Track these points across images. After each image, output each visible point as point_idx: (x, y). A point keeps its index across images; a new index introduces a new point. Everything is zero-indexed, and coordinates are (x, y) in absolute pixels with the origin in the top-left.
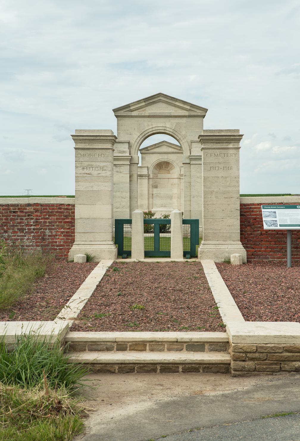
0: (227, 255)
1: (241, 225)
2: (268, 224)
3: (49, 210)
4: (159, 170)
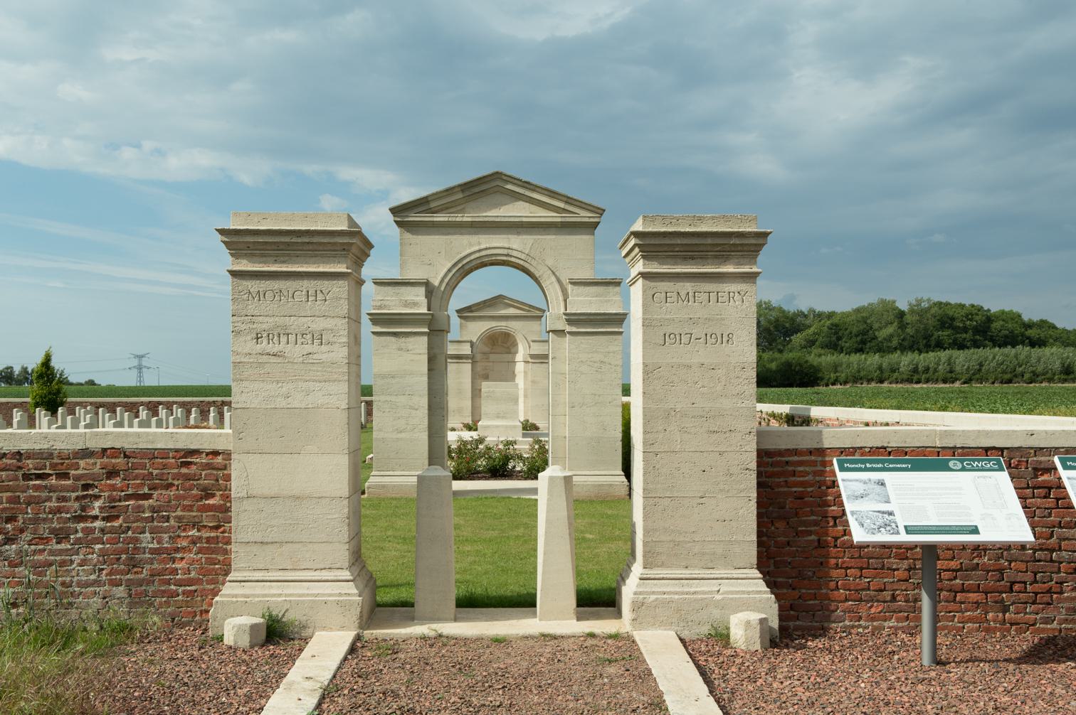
0: (716, 613)
1: (759, 516)
2: (865, 525)
3: (151, 470)
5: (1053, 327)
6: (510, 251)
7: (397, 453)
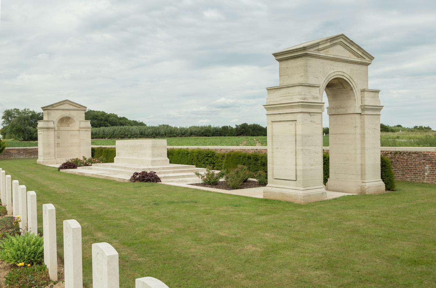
4: (60, 123)
5: (127, 119)
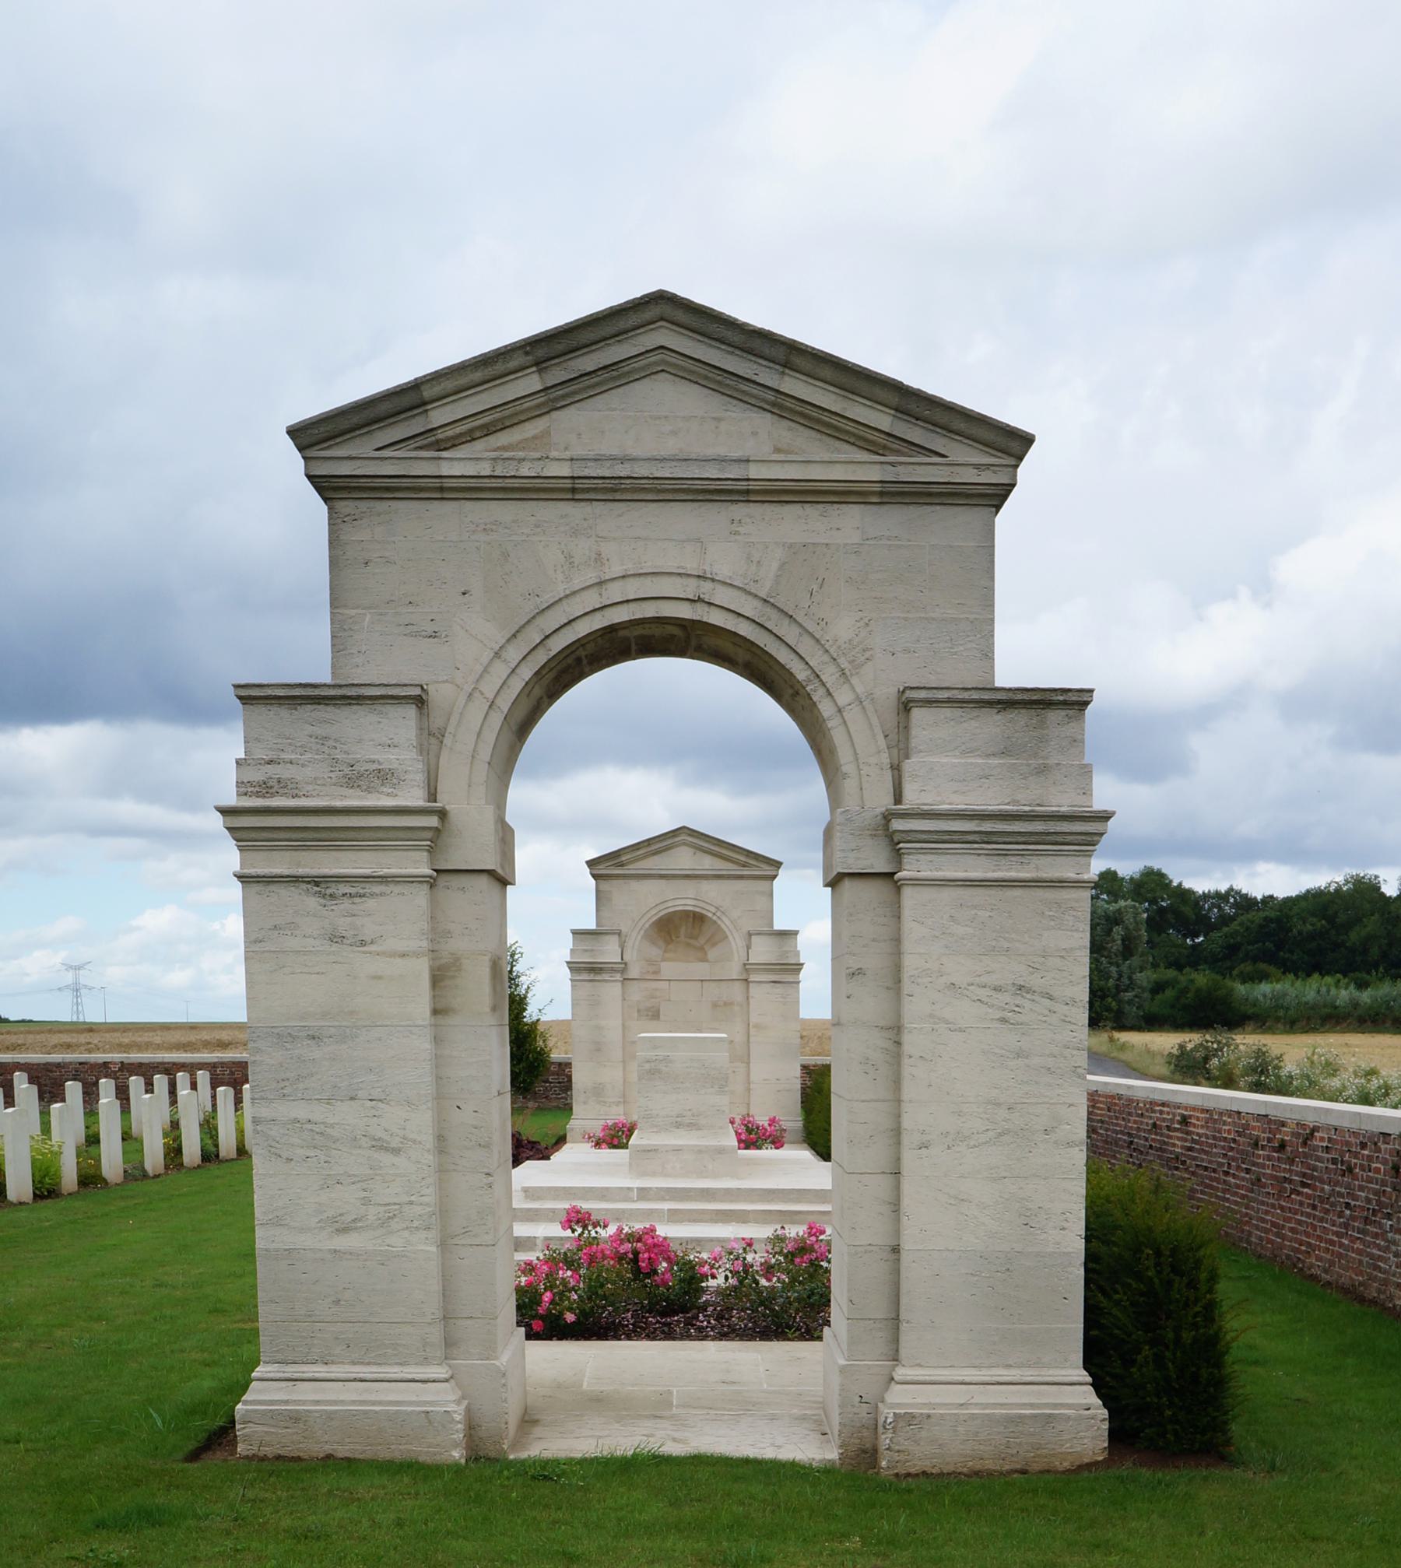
6: (707, 586)
7: (337, 1302)
